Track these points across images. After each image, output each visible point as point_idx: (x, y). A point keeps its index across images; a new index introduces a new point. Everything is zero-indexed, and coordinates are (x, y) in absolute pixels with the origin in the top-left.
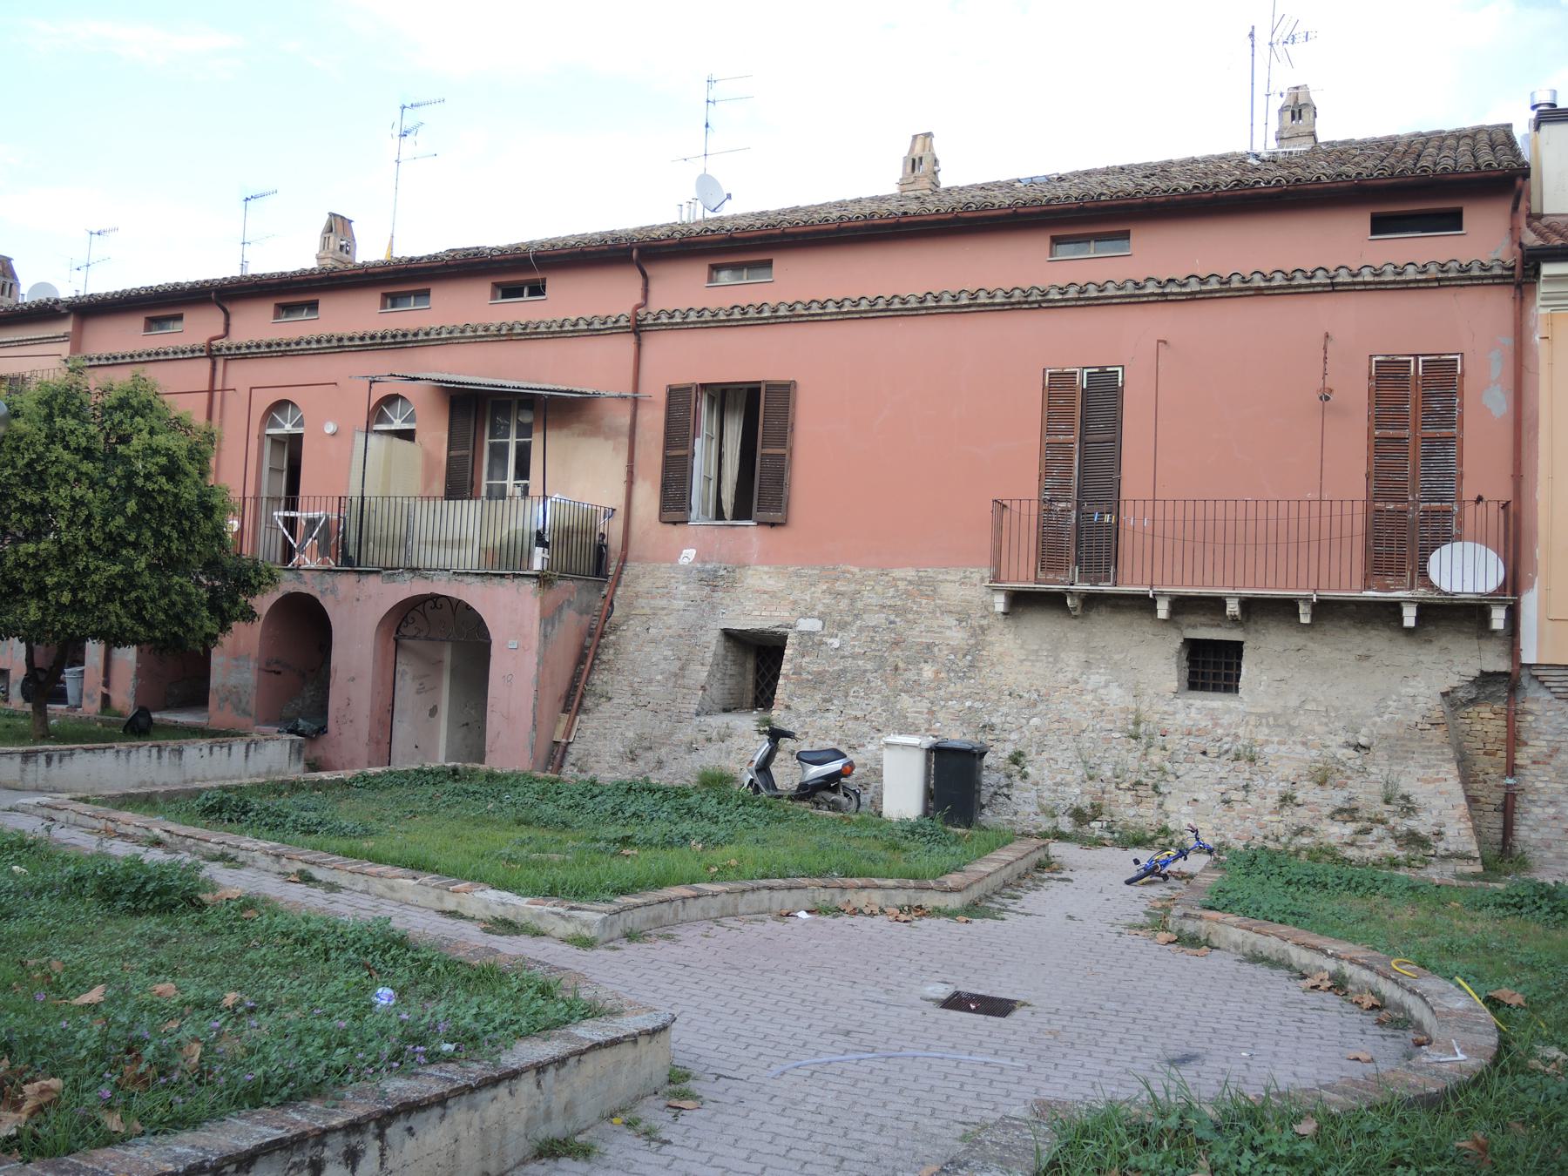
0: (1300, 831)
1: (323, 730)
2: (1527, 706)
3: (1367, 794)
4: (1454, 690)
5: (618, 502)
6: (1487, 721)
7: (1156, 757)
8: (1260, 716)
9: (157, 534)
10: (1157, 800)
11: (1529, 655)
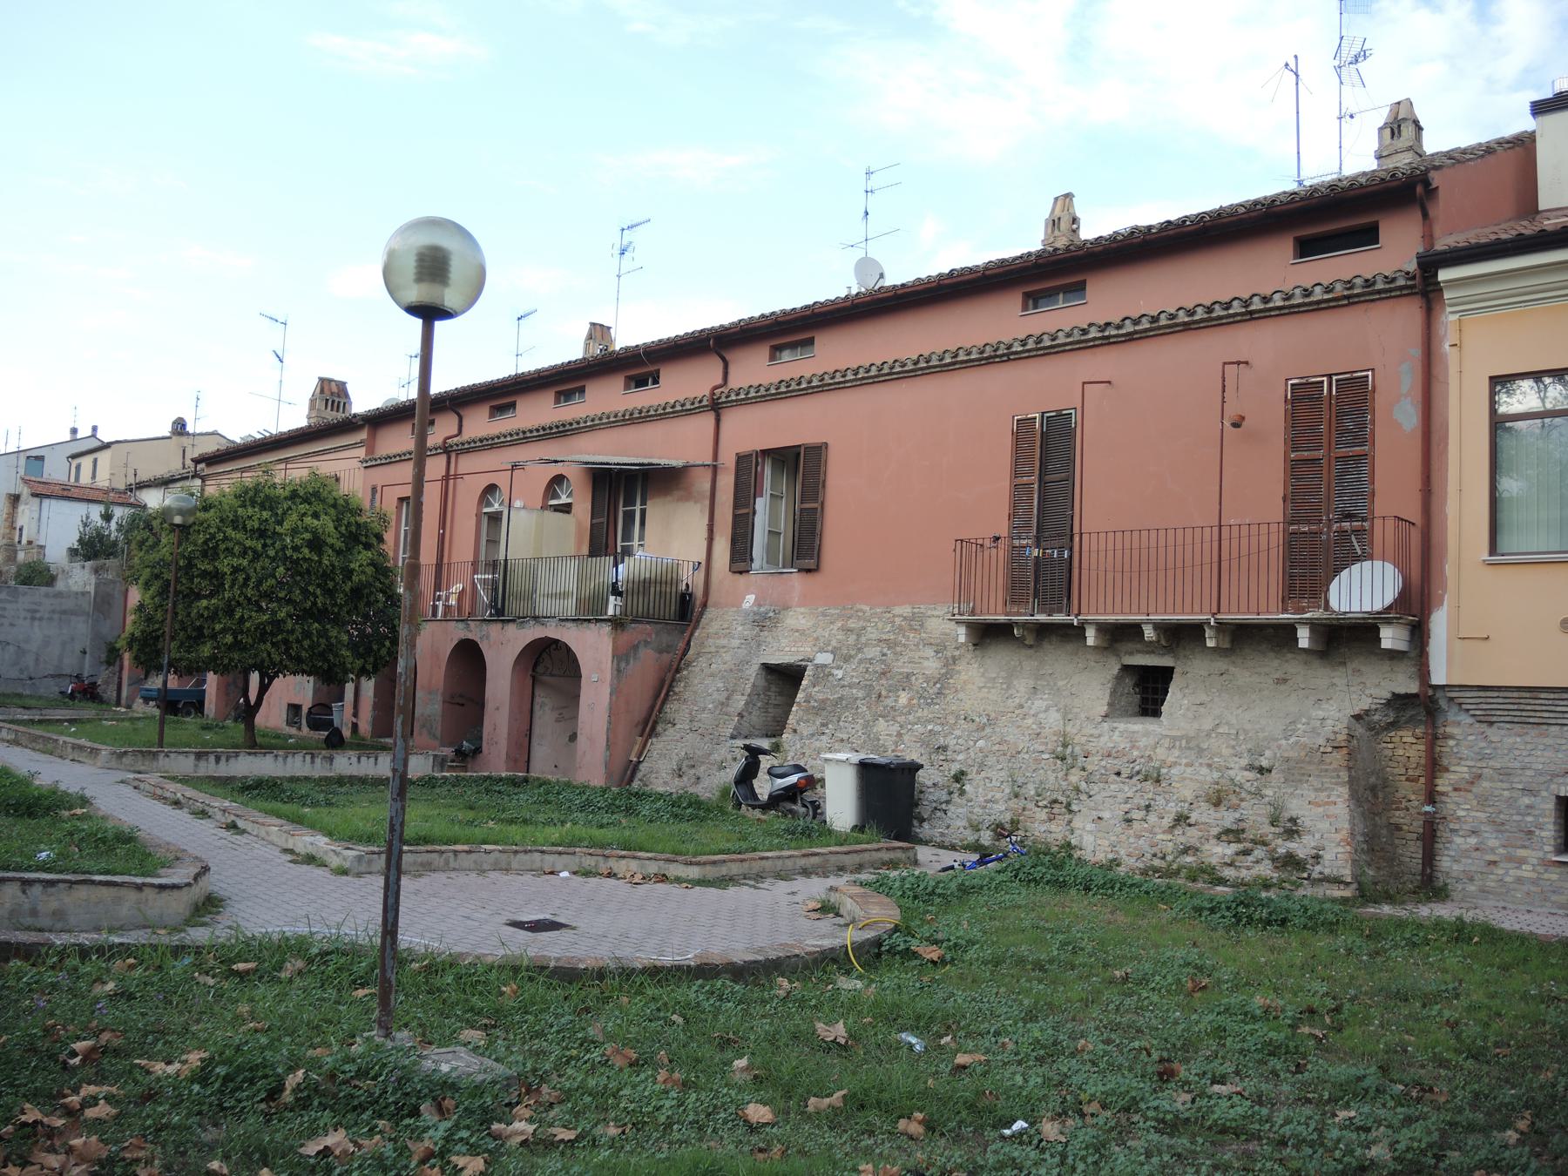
0: (1186, 851)
1: (478, 750)
2: (1448, 730)
3: (1255, 816)
4: (1367, 712)
5: (702, 558)
6: (1407, 746)
7: (1075, 777)
8: (1174, 738)
9: (304, 591)
10: (1068, 817)
11: (1438, 678)
